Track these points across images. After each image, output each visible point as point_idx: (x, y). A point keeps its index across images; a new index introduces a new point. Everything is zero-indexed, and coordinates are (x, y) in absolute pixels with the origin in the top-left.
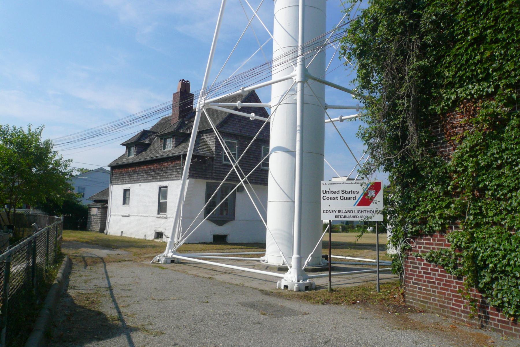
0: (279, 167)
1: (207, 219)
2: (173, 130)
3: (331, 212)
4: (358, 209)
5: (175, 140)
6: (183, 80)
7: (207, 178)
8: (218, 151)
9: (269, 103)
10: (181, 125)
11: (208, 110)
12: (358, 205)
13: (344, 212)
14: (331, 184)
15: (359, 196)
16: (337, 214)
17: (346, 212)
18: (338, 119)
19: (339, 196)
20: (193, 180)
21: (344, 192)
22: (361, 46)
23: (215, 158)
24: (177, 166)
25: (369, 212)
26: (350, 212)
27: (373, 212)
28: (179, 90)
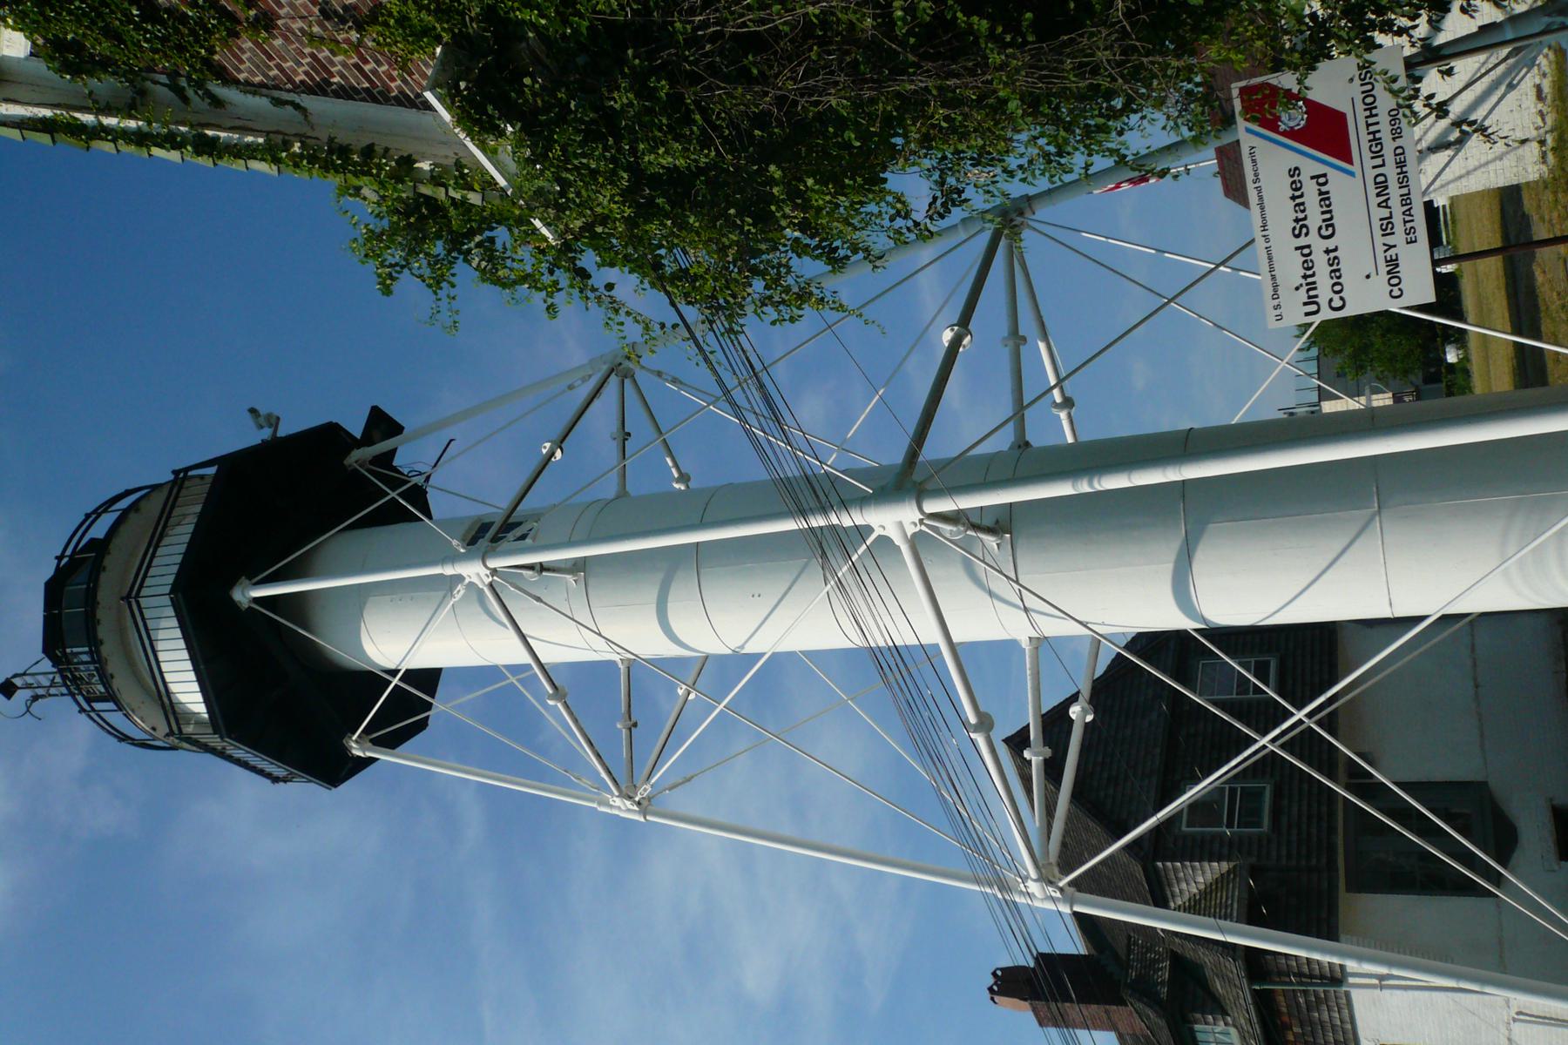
0: (1255, 586)
1: (1505, 866)
2: (1162, 1023)
3: (1393, 263)
4: (1367, 155)
5: (1198, 1016)
6: (991, 989)
7: (1333, 888)
8: (1225, 851)
9: (1025, 644)
10: (1144, 991)
11: (1066, 866)
12: (1350, 162)
13: (1385, 213)
14: (1275, 287)
15: (1311, 164)
16: (1399, 238)
17: (1384, 204)
18: (1063, 415)
19: (1319, 246)
20: (1342, 937)
21: (1300, 228)
22: (727, 218)
23: (1253, 860)
24: (1298, 1004)
25: (1370, 108)
26: (1382, 187)
27: (1367, 94)
28: (1026, 1004)
